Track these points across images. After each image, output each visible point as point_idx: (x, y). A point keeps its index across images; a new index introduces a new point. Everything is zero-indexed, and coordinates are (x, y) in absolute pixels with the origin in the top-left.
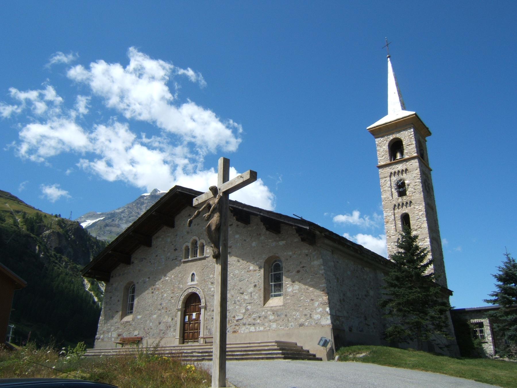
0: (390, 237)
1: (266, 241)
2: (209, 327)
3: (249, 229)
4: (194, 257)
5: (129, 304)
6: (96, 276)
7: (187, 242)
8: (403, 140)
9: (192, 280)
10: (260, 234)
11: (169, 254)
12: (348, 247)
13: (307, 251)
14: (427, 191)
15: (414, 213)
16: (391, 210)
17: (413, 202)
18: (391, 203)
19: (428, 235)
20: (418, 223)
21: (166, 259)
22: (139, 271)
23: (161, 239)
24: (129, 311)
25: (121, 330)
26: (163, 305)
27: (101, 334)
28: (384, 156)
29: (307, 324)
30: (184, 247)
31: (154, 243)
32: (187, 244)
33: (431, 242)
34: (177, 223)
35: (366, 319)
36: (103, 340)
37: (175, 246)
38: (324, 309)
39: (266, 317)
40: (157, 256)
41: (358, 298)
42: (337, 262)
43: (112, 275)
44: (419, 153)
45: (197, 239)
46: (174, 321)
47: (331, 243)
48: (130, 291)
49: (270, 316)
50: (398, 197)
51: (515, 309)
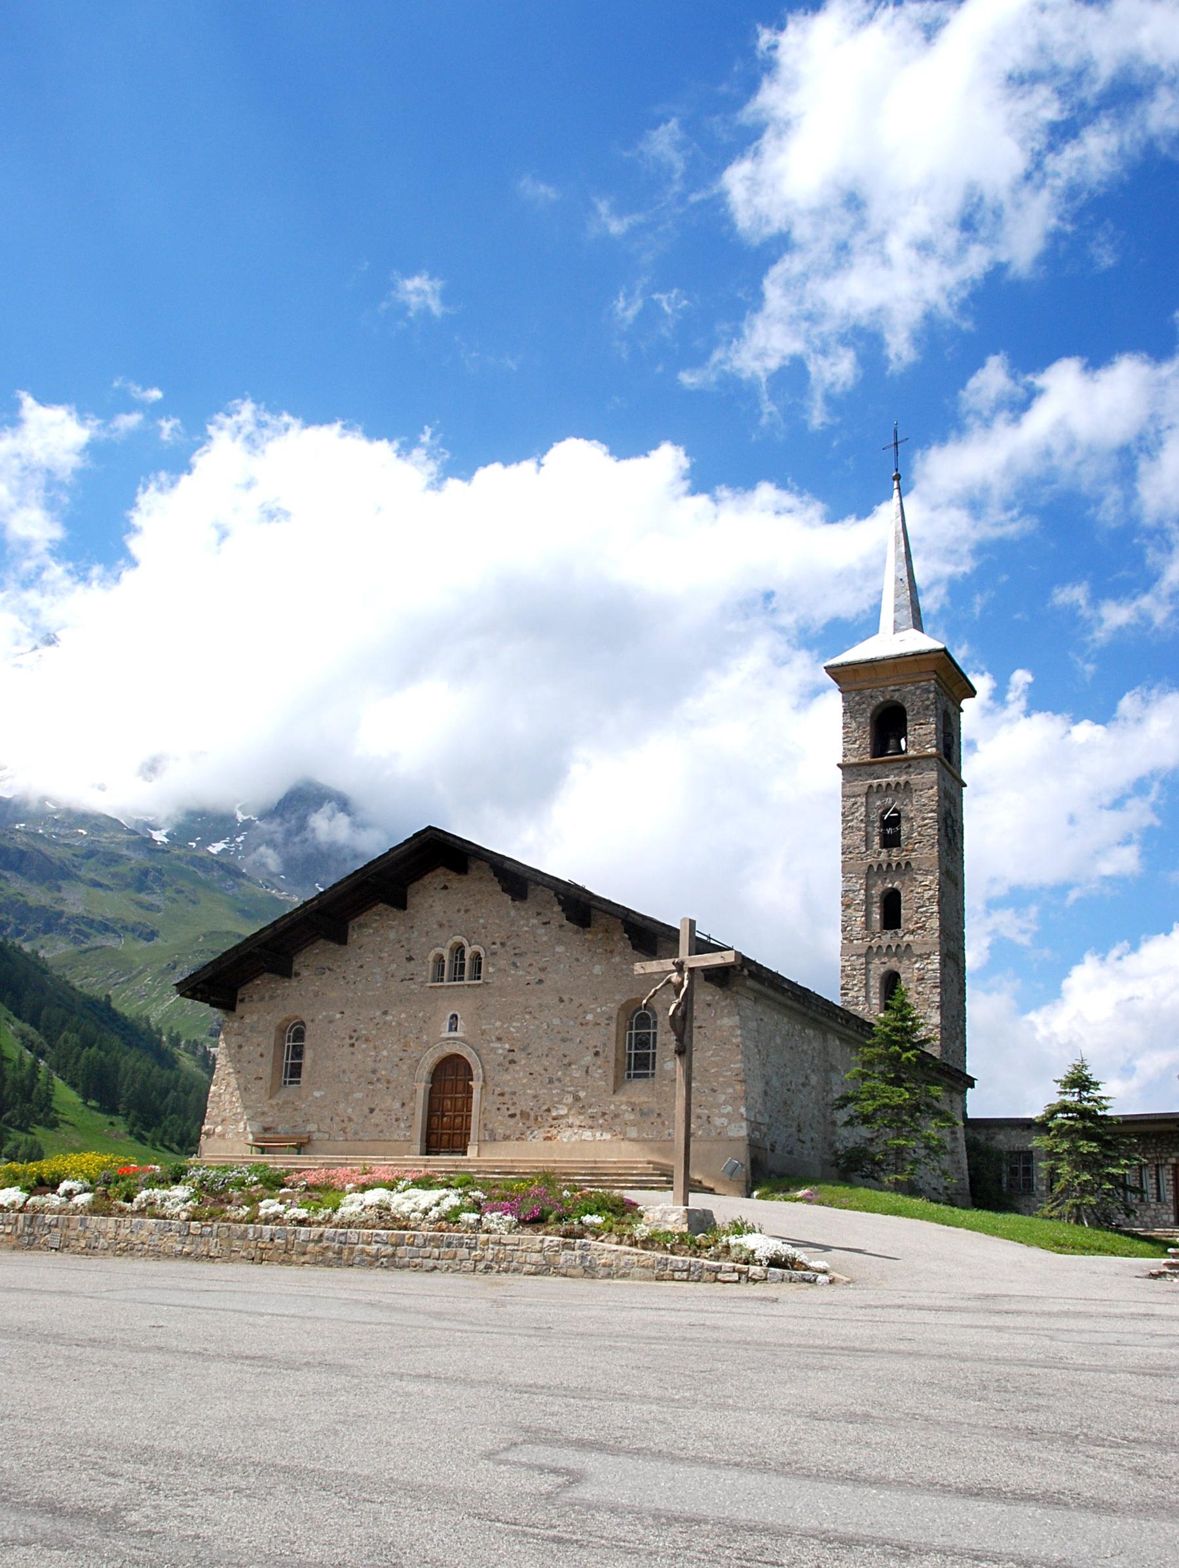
0: (852, 941)
1: (624, 967)
2: (490, 1126)
3: (586, 937)
4: (455, 980)
5: (287, 1064)
6: (212, 998)
7: (437, 945)
8: (907, 710)
9: (453, 1027)
10: (612, 952)
11: (394, 966)
12: (783, 991)
13: (709, 998)
14: (949, 841)
15: (912, 891)
16: (861, 878)
17: (913, 864)
18: (862, 859)
19: (938, 948)
20: (919, 916)
21: (387, 978)
22: (316, 994)
23: (371, 931)
24: (288, 1080)
25: (271, 1119)
26: (378, 1075)
27: (216, 1124)
28: (858, 742)
29: (700, 1133)
30: (432, 954)
31: (353, 936)
32: (439, 950)
33: (943, 963)
34: (412, 900)
35: (799, 1131)
36: (222, 1136)
37: (409, 951)
38: (736, 1109)
39: (616, 1116)
40: (361, 967)
41: (789, 1090)
42: (761, 1020)
43: (239, 997)
44: (941, 746)
45: (465, 942)
46: (407, 1109)
47: (757, 986)
48: (289, 1036)
49: (627, 1114)
50: (882, 847)
51: (406, 1157)
